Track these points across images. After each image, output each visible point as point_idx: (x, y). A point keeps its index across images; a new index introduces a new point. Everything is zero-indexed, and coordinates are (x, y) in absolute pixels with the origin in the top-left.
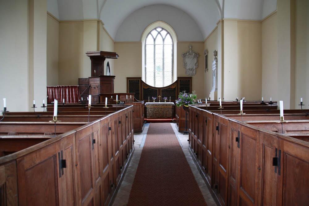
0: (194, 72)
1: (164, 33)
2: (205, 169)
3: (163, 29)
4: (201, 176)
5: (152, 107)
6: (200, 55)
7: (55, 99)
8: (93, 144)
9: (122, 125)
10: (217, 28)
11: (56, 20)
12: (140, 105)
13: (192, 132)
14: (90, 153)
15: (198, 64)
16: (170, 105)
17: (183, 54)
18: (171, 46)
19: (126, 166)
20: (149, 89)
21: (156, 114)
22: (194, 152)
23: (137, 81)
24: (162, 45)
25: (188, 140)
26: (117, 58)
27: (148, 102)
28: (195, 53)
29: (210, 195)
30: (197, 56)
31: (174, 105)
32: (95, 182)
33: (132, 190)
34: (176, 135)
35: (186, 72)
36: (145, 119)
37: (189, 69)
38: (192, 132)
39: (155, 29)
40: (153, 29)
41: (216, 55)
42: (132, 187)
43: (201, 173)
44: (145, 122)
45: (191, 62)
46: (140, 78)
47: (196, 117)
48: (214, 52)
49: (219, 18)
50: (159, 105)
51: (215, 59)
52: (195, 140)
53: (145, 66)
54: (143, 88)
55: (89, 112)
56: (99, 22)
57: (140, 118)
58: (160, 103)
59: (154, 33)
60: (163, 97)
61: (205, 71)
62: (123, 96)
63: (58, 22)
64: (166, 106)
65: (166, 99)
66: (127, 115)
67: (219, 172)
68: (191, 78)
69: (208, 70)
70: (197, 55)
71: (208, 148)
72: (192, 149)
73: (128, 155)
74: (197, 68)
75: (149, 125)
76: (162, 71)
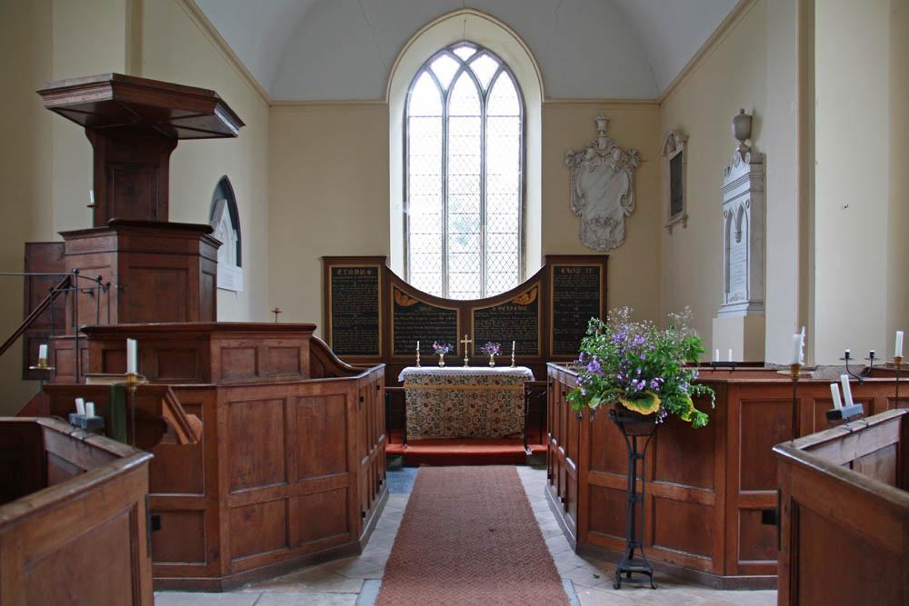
0: (619, 235)
1: (485, 67)
3: (481, 49)
5: (432, 388)
6: (641, 161)
12: (345, 396)
16: (512, 378)
17: (570, 152)
18: (517, 123)
20: (422, 309)
21: (450, 419)
23: (369, 272)
24: (478, 121)
26: (231, 135)
27: (414, 365)
28: (625, 153)
30: (633, 162)
31: (533, 380)
34: (567, 588)
35: (582, 237)
36: (392, 448)
37: (597, 221)
39: (449, 49)
40: (440, 48)
42: (404, 515)
44: (399, 461)
45: (603, 191)
46: (383, 260)
48: (737, 120)
50: (464, 378)
52: (567, 474)
53: (405, 207)
54: (395, 303)
57: (347, 470)
58: (466, 369)
59: (445, 66)
60: (480, 342)
61: (670, 227)
62: (234, 343)
64: (497, 383)
65: (494, 350)
66: (363, 395)
68: (604, 259)
69: (685, 218)
70: (632, 161)
73: (381, 483)
74: (632, 214)
75: (410, 487)
76: (478, 231)
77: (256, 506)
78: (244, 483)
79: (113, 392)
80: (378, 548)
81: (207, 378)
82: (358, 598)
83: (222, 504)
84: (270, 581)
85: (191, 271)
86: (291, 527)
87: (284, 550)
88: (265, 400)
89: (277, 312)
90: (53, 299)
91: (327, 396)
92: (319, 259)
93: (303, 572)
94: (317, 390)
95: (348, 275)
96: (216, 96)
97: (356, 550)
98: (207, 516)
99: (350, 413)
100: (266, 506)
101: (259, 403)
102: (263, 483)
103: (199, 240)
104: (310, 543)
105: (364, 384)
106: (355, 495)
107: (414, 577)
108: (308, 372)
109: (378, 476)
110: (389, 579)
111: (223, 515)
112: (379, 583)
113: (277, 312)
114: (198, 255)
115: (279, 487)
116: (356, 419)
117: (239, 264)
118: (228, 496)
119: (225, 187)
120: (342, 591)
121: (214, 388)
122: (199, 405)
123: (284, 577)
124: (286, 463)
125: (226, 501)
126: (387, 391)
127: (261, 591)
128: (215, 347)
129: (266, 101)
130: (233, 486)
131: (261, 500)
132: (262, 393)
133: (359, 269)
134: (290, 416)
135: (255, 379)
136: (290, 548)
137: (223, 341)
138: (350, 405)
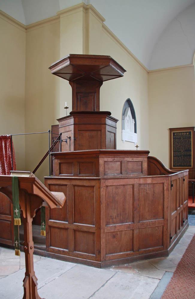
7: (149, 156)
11: (21, 26)
12: (163, 183)
23: (188, 134)
26: (121, 76)
33: (181, 261)
62: (110, 159)
63: (24, 30)
77: (119, 232)
78: (113, 222)
79: (13, 180)
80: (177, 254)
81: (98, 175)
82: (159, 282)
83: (102, 231)
84: (123, 266)
85: (102, 131)
86: (135, 243)
87: (132, 252)
88: (124, 185)
89: (137, 147)
90: (54, 146)
91: (154, 184)
92: (168, 129)
93: (139, 263)
94: (149, 181)
95: (179, 135)
96: (110, 58)
97: (166, 254)
98: (96, 235)
99: (165, 192)
100: (123, 232)
101: (121, 186)
102: (122, 222)
103: (106, 118)
104: (144, 250)
105: (173, 178)
106: (167, 229)
107: (190, 274)
108: (146, 173)
109: (182, 219)
110: (177, 273)
111: (102, 235)
112: (171, 275)
113: (137, 147)
114: (105, 124)
115: (129, 224)
116: (169, 196)
117: (135, 132)
118: (105, 227)
119: (129, 102)
120: (153, 277)
121: (99, 179)
122: (93, 187)
123: (130, 264)
124: (133, 214)
125: (104, 230)
126: (189, 182)
127: (117, 270)
128: (101, 161)
129: (146, 71)
130: (108, 223)
131: (121, 230)
132: (122, 182)
133: (183, 132)
134: (135, 193)
135: (121, 175)
136: (134, 252)
137: (105, 158)
138: (165, 188)
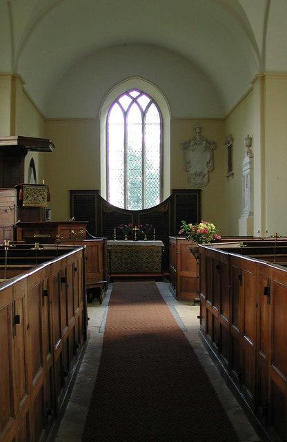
0: (206, 180)
1: (144, 101)
2: (240, 375)
3: (142, 93)
4: (228, 390)
8: (14, 325)
9: (67, 286)
10: (252, 89)
13: (207, 299)
14: (9, 345)
15: (213, 163)
19: (74, 370)
22: (213, 340)
24: (141, 126)
25: (198, 317)
28: (208, 142)
29: (252, 429)
32: (19, 405)
38: (207, 299)
39: (127, 93)
41: (251, 146)
43: (229, 383)
45: (198, 160)
46: (98, 192)
47: (217, 268)
49: (255, 72)
51: (248, 153)
52: (213, 316)
55: (6, 258)
56: (14, 78)
59: (125, 101)
61: (228, 177)
67: (272, 382)
68: (199, 191)
70: (211, 146)
71: (245, 333)
72: (208, 335)
